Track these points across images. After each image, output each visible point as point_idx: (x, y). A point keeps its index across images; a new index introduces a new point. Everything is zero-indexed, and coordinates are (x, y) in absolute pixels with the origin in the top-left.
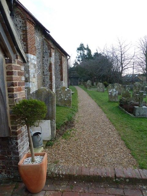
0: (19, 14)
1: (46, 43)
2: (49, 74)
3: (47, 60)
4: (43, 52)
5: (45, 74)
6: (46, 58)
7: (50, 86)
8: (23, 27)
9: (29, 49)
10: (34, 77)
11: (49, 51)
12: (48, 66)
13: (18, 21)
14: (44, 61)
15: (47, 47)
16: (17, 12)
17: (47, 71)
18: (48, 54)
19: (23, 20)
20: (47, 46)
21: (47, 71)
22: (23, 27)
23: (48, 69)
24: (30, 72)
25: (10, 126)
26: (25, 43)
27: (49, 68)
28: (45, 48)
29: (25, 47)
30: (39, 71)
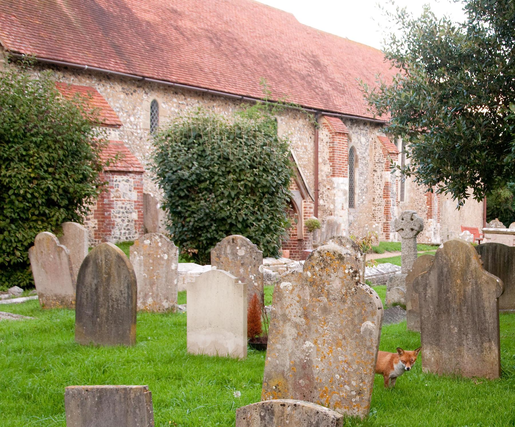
0: (326, 126)
1: (381, 144)
2: (384, 203)
3: (381, 177)
4: (375, 160)
5: (377, 202)
6: (379, 173)
7: (384, 227)
8: (330, 143)
9: (337, 171)
10: (343, 209)
11: (385, 159)
12: (382, 188)
13: (324, 135)
14: (375, 177)
15: (381, 152)
16: (323, 123)
17: (381, 197)
18: (384, 165)
19: (331, 133)
20: (381, 150)
21: (381, 197)
22: (330, 143)
23: (382, 193)
24: (336, 202)
25: (303, 234)
26: (331, 164)
27: (384, 191)
28: (377, 154)
29: (332, 168)
30: (364, 197)
